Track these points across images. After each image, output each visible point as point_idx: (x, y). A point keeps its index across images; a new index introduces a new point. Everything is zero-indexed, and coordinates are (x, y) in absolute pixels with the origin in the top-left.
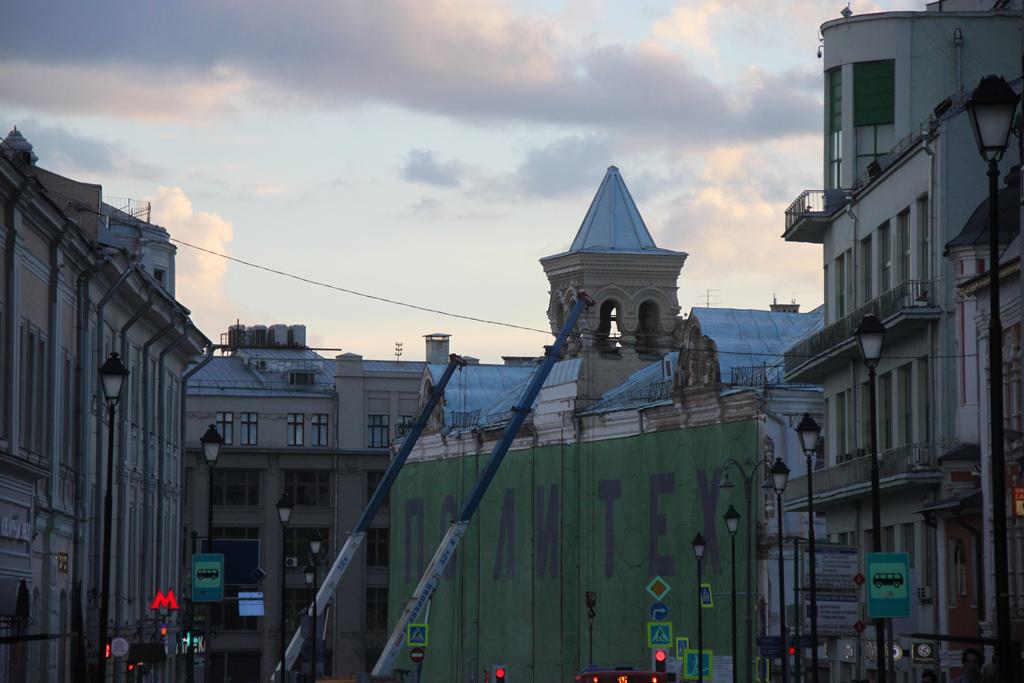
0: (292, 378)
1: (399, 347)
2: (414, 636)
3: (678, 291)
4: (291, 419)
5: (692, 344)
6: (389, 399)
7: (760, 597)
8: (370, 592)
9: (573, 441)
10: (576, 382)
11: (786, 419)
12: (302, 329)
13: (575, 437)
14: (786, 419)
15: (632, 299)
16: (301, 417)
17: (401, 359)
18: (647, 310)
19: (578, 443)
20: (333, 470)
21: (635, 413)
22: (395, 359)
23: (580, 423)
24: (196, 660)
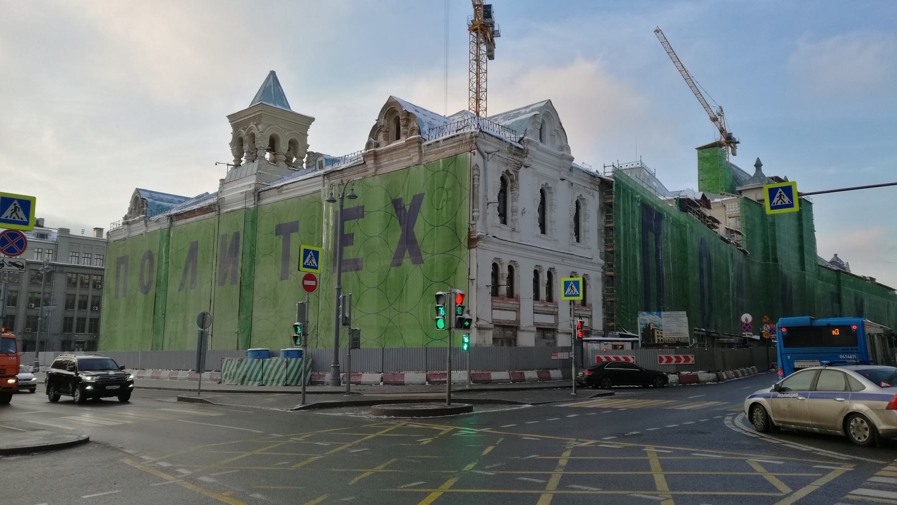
0: (38, 235)
1: (83, 231)
2: (775, 200)
3: (308, 137)
4: (36, 250)
5: (386, 121)
6: (79, 246)
7: (243, 317)
8: (66, 319)
9: (253, 206)
10: (255, 174)
11: (486, 154)
12: (43, 220)
13: (254, 204)
14: (486, 154)
15: (286, 135)
16: (41, 250)
17: (84, 235)
18: (293, 144)
19: (257, 207)
20: (53, 271)
21: (321, 178)
22: (81, 235)
23: (259, 196)
24: (657, 342)
